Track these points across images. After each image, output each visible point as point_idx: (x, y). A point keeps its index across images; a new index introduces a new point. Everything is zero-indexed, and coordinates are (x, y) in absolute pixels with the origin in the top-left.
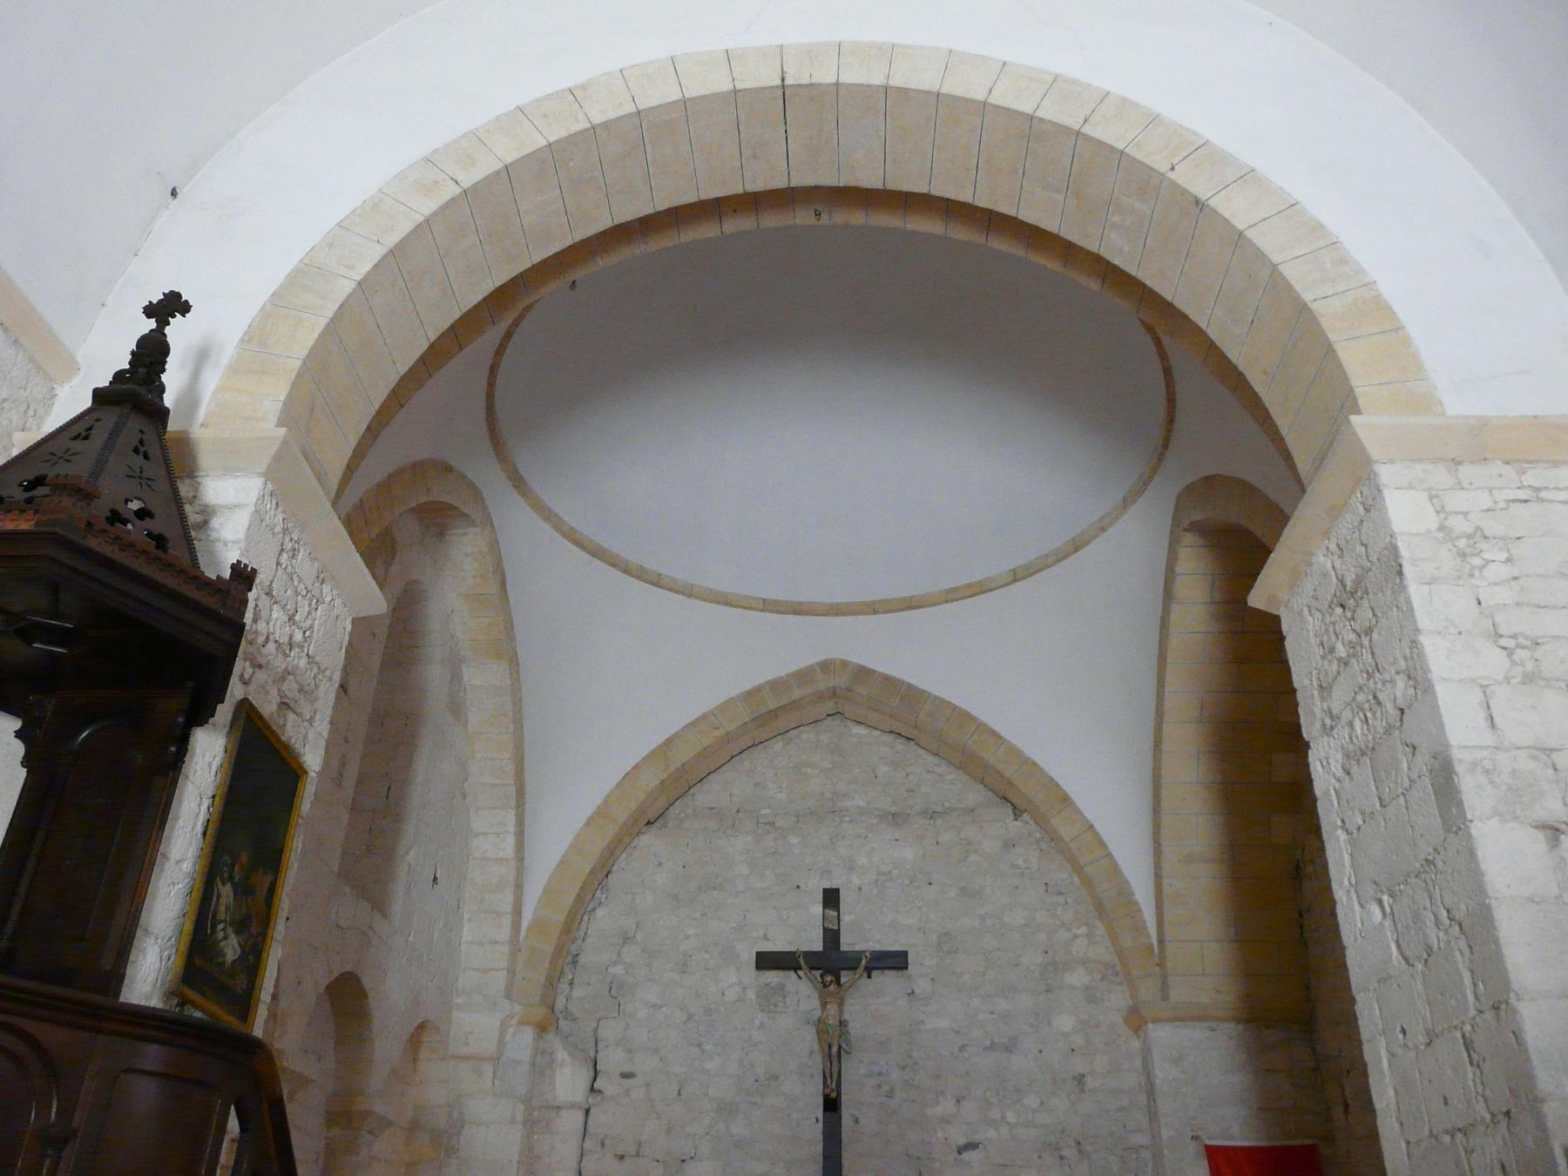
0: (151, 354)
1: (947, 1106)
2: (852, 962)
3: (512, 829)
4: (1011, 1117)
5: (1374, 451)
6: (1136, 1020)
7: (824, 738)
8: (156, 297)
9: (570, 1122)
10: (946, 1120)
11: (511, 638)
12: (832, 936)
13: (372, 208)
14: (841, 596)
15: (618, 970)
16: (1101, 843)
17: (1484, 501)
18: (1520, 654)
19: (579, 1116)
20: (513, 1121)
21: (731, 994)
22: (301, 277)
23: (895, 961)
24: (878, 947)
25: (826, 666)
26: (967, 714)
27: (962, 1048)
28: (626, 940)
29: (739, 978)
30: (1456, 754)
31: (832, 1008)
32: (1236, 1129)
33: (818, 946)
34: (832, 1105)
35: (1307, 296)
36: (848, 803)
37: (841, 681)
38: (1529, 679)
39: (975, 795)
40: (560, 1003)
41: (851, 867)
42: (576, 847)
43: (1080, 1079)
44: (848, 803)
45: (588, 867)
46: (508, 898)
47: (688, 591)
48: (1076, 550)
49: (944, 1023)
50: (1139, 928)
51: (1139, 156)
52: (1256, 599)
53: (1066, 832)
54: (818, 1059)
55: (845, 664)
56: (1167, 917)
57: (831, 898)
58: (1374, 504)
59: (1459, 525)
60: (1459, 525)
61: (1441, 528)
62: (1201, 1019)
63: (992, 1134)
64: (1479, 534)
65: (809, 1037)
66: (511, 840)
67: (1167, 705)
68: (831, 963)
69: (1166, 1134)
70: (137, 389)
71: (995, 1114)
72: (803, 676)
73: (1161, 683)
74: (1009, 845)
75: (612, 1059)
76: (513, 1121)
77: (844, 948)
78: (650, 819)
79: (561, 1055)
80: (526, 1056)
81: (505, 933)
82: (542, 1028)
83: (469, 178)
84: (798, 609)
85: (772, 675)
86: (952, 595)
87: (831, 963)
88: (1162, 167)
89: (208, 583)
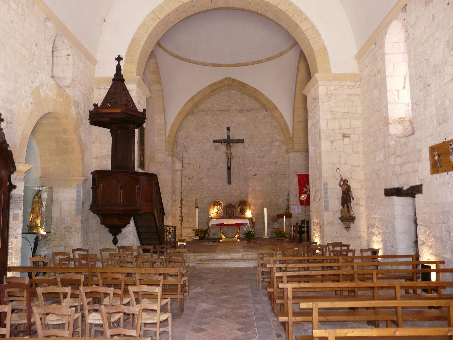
0: (119, 68)
1: (251, 168)
2: (233, 141)
3: (163, 118)
4: (263, 169)
5: (318, 79)
6: (287, 152)
7: (226, 93)
8: (117, 57)
9: (179, 173)
10: (250, 170)
11: (160, 79)
12: (229, 137)
13: (143, 25)
14: (229, 62)
15: (186, 144)
16: (283, 117)
17: (334, 88)
18: (334, 114)
19: (180, 172)
20: (169, 173)
21: (209, 148)
22: (134, 41)
23: (242, 141)
24: (238, 138)
25: (226, 79)
26: (257, 90)
27: (254, 157)
28: (187, 137)
29: (210, 145)
30: (321, 130)
31: (229, 151)
32: (303, 171)
33: (226, 138)
34: (229, 168)
35: (313, 47)
36: (232, 108)
37: (230, 83)
38: (334, 119)
39: (258, 106)
40: (175, 150)
41: (232, 122)
42: (176, 120)
43: (276, 163)
44: (232, 108)
45: (179, 124)
46: (164, 131)
47: (196, 63)
48: (281, 55)
49: (251, 153)
50: (289, 134)
51: (287, 13)
52: (304, 93)
53: (276, 115)
54: (226, 160)
55: (231, 78)
56: (294, 133)
57: (228, 129)
58: (317, 88)
59: (329, 92)
60: (329, 92)
61: (327, 93)
62: (299, 152)
63: (259, 173)
64: (332, 94)
65: (225, 155)
66: (163, 120)
67: (297, 92)
68: (228, 142)
69: (291, 172)
70: (118, 79)
71: (260, 169)
72: (221, 81)
73: (296, 86)
74: (264, 117)
75: (186, 161)
76: (169, 173)
77: (231, 139)
78: (191, 113)
79: (176, 161)
80: (170, 161)
81: (164, 139)
82: (172, 156)
83: (162, 17)
84: (220, 66)
85: (215, 81)
86: (254, 63)
87: (228, 142)
88: (291, 16)
89: (139, 112)
